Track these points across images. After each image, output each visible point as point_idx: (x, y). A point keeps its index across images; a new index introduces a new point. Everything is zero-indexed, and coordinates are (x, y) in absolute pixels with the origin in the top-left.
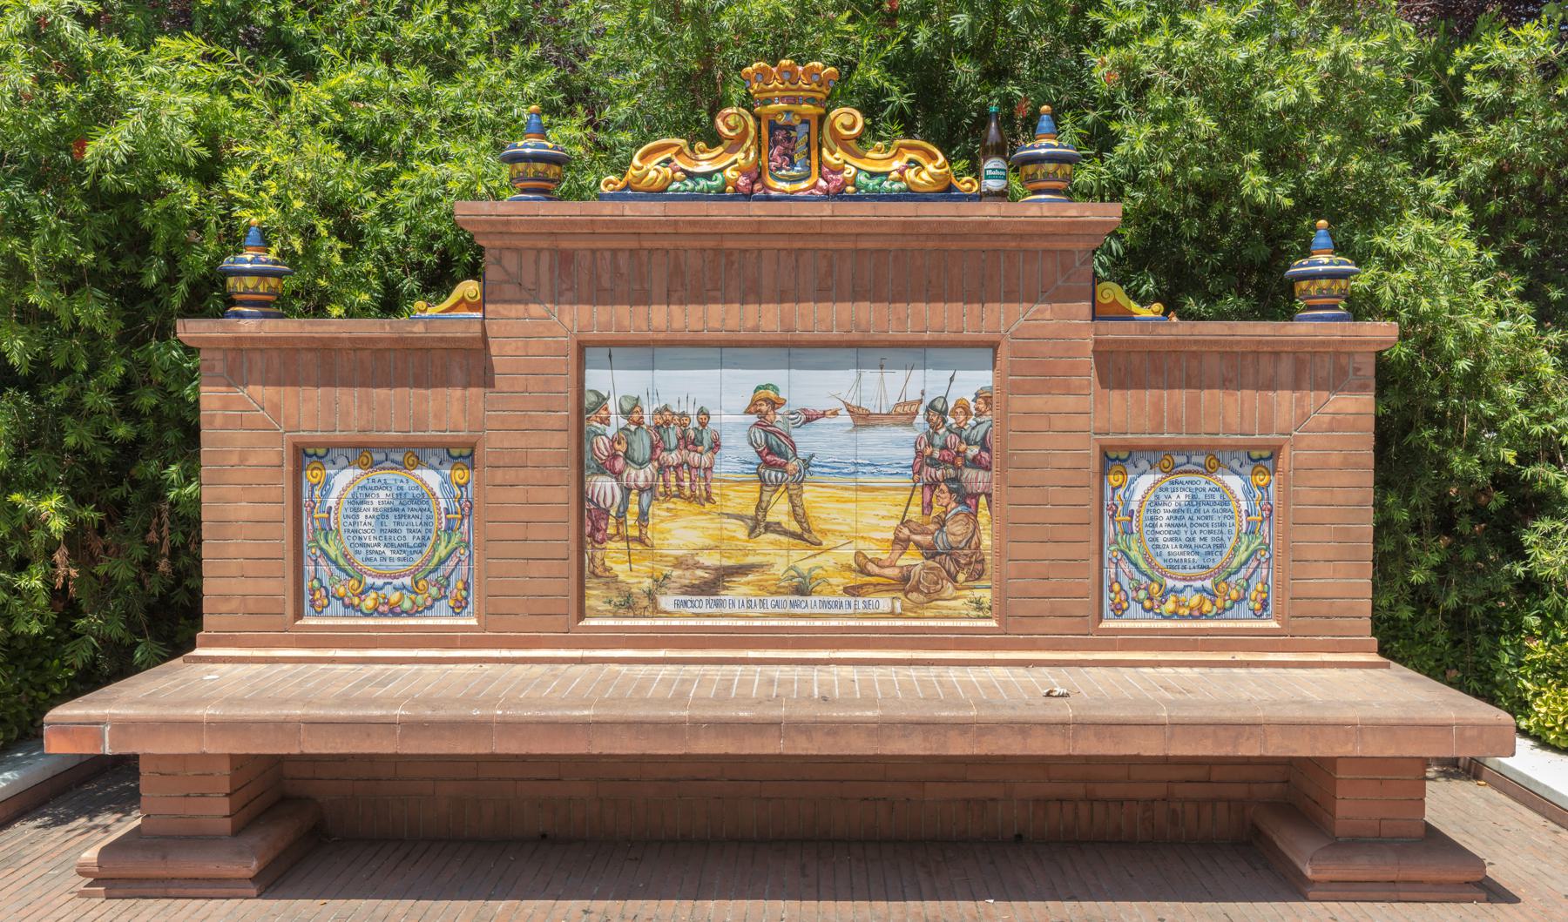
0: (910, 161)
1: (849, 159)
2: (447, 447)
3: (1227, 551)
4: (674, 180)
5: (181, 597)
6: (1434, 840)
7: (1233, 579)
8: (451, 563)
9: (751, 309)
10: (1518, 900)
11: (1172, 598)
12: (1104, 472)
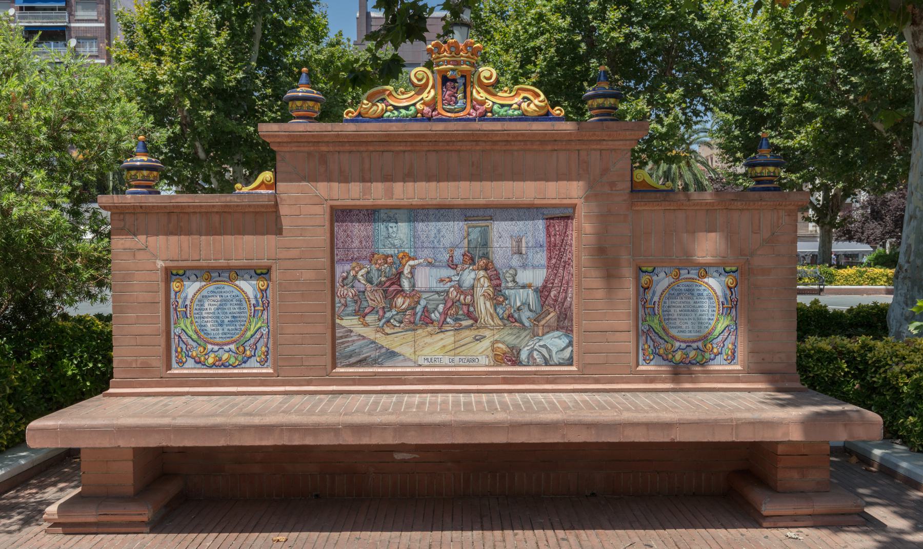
0: (524, 98)
1: (488, 97)
4: (386, 111)
8: (258, 336)
9: (410, 185)
12: (168, 282)
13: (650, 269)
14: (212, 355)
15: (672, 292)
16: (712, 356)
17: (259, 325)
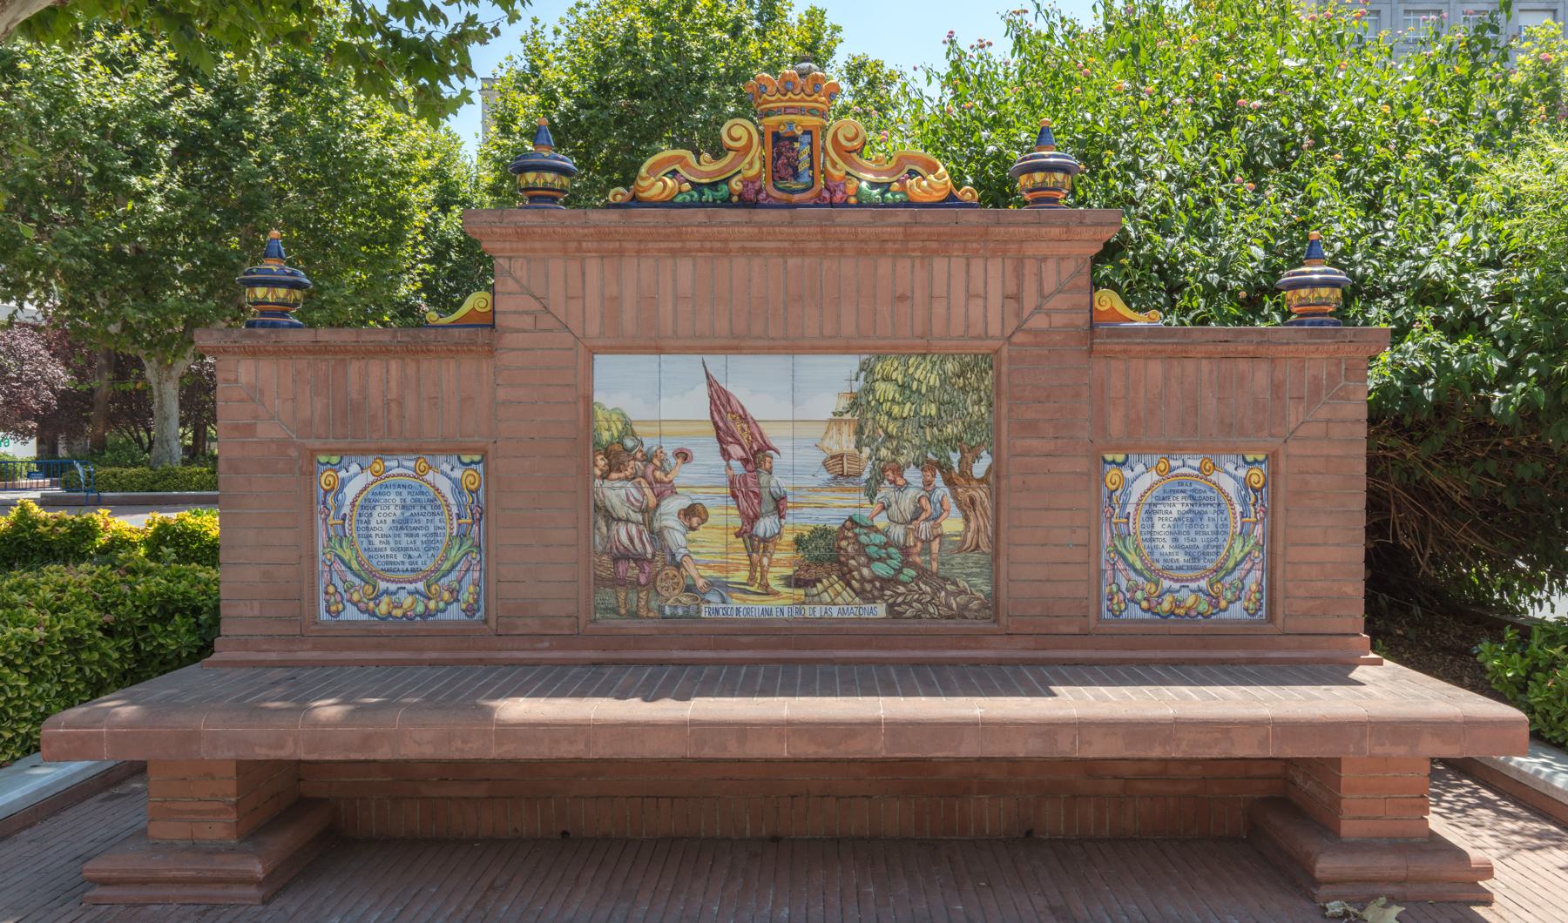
5: (1383, 599)
7: (1228, 579)
11: (385, 599)
13: (1120, 458)
16: (441, 605)
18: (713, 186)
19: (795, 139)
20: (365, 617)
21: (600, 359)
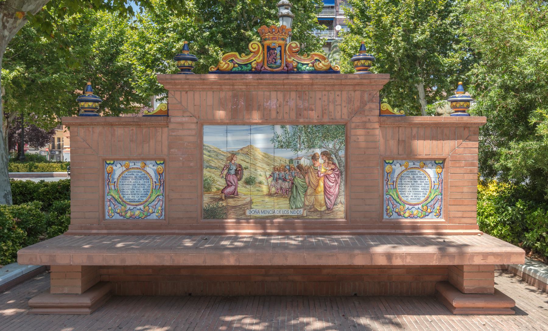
0: (316, 60)
2: (435, 160)
3: (148, 197)
6: (498, 295)
10: (527, 314)
13: (391, 162)
14: (408, 211)
15: (401, 176)
17: (436, 194)
18: (246, 65)
19: (275, 49)
20: (122, 218)
21: (205, 127)
